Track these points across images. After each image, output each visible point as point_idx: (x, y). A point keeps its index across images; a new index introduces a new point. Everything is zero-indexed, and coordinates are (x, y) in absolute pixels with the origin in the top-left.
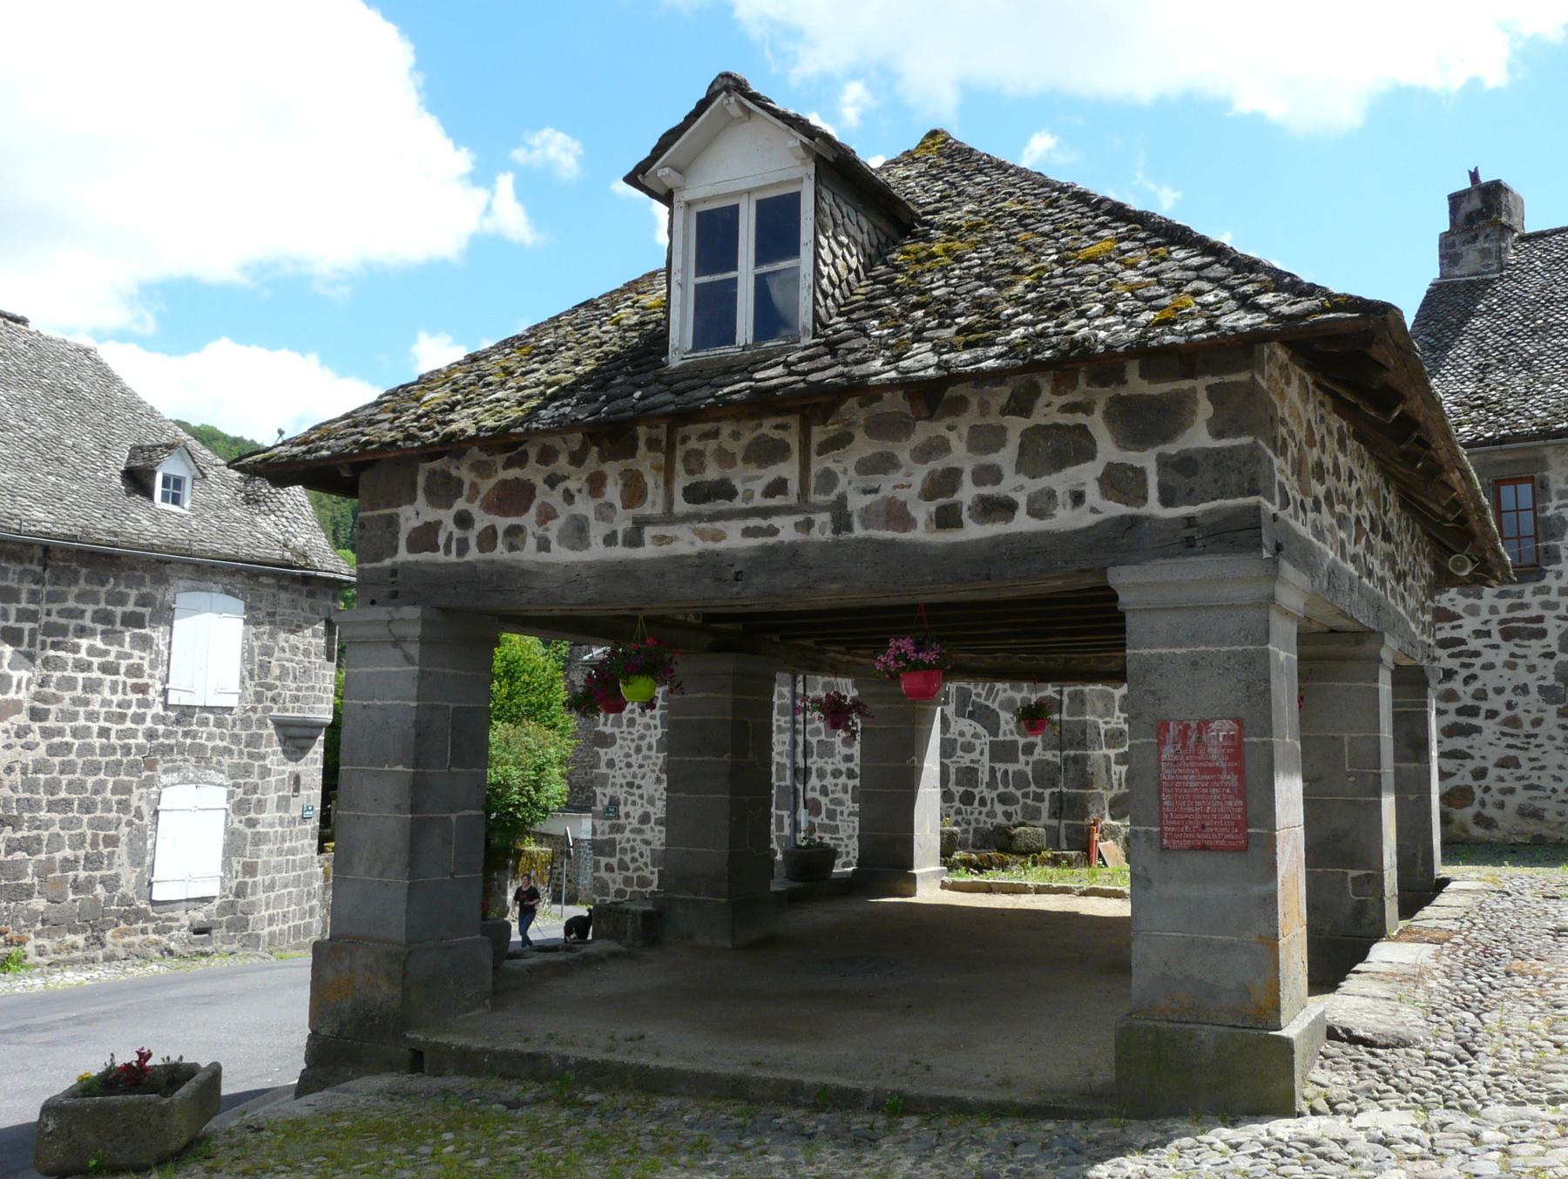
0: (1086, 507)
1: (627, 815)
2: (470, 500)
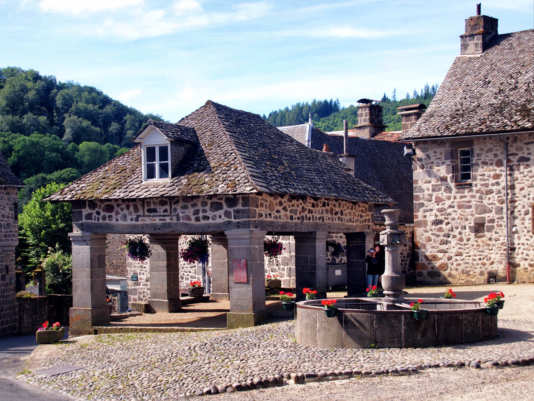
0: (221, 219)
1: (141, 279)
2: (100, 208)
